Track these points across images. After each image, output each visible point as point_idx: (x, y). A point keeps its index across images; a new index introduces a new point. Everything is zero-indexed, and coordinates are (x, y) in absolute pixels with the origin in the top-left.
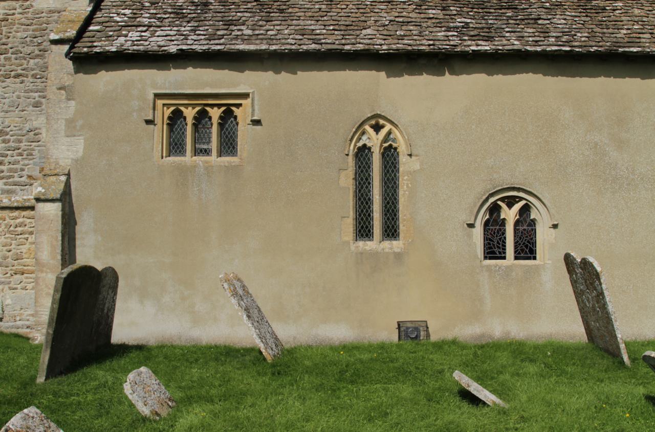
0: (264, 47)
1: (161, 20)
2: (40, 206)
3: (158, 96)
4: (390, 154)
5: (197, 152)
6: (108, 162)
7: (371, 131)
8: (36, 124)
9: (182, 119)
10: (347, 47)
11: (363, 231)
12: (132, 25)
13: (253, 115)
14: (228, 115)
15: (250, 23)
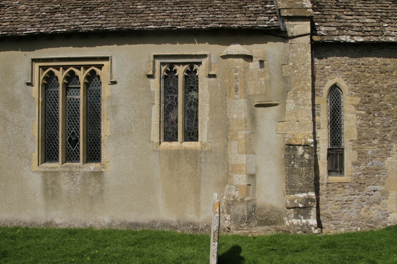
3: (156, 57)
6: (375, 142)
9: (76, 78)
13: (111, 78)
14: (92, 77)
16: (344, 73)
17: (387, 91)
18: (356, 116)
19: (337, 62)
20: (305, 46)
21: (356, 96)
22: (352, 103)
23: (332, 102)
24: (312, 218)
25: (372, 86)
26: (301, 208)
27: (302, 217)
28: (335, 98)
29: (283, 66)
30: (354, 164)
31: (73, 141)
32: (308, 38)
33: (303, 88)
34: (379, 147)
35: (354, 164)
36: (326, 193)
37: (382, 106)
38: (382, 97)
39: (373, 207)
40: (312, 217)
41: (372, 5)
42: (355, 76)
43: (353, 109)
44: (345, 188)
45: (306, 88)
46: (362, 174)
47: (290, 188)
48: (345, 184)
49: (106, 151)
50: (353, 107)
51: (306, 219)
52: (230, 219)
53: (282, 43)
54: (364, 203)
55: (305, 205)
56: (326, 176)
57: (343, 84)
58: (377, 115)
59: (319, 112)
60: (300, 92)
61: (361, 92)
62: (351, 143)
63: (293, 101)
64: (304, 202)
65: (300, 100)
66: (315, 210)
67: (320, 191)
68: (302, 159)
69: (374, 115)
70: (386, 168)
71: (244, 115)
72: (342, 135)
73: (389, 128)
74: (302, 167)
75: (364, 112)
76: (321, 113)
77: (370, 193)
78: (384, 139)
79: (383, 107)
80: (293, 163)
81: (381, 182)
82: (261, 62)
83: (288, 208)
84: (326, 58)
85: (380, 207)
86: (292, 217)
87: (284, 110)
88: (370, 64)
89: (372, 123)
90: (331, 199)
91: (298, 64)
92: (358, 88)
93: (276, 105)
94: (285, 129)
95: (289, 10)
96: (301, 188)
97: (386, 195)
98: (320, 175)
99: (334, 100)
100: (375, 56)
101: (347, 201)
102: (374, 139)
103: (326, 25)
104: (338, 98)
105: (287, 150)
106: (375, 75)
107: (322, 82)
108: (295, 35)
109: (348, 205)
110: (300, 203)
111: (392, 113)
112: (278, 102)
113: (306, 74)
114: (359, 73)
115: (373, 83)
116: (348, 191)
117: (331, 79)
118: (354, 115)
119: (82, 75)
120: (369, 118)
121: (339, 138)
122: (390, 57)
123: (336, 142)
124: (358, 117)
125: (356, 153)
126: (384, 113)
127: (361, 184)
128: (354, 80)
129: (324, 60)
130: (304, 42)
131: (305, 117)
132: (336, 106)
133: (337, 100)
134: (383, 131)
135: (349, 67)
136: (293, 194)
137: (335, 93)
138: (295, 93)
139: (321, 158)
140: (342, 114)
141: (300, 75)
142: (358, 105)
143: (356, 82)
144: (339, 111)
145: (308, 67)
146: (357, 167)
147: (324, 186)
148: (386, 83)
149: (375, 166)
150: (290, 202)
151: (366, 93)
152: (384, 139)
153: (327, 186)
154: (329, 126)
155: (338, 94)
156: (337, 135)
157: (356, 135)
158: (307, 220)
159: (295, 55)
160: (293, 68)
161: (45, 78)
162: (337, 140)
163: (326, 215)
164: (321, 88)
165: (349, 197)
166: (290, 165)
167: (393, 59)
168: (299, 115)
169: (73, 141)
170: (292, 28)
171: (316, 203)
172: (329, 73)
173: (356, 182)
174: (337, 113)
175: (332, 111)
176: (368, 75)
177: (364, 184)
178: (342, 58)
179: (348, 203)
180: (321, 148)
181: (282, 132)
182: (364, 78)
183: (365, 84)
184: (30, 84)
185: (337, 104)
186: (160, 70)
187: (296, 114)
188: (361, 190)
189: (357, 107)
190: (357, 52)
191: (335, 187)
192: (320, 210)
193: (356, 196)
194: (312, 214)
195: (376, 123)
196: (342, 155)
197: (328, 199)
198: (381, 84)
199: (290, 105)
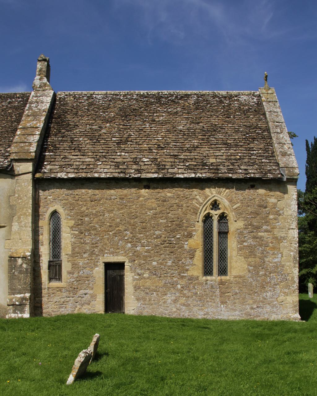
6: (85, 255)
16: (62, 202)
17: (96, 215)
18: (71, 235)
19: (57, 193)
20: (27, 181)
21: (71, 219)
22: (67, 225)
23: (54, 225)
24: (26, 313)
25: (83, 212)
26: (17, 305)
27: (19, 312)
28: (56, 221)
29: (11, 197)
30: (69, 273)
32: (30, 176)
33: (25, 214)
34: (88, 260)
35: (69, 273)
36: (47, 295)
37: (91, 227)
38: (92, 221)
39: (84, 307)
40: (26, 312)
41: (99, 146)
42: (71, 204)
43: (68, 230)
44: (62, 292)
45: (28, 214)
46: (75, 280)
47: (11, 290)
48: (62, 289)
50: (68, 228)
51: (21, 314)
53: (11, 179)
54: (77, 304)
55: (20, 303)
56: (47, 282)
57: (61, 210)
58: (87, 235)
59: (42, 232)
60: (23, 217)
61: (75, 217)
62: (67, 256)
63: (17, 224)
64: (20, 300)
65: (23, 223)
66: (29, 307)
67: (43, 294)
68: (21, 268)
69: (85, 235)
70: (94, 276)
72: (61, 250)
73: (97, 245)
74: (21, 274)
75: (77, 232)
76: (44, 233)
77: (82, 296)
78: (92, 253)
79: (92, 228)
80: (13, 271)
81: (90, 287)
83: (9, 305)
84: (49, 191)
85: (90, 307)
86: (11, 312)
87: (10, 231)
88: (83, 194)
89: (83, 241)
90: (51, 300)
91: (22, 195)
92: (73, 213)
93: (4, 227)
94: (11, 245)
95: (17, 154)
96: (20, 290)
97: (94, 298)
98: (42, 282)
99: (55, 223)
100: (86, 188)
101: (63, 302)
102: (85, 253)
103: (53, 164)
104: (58, 221)
105: (10, 261)
106: (87, 203)
107: (45, 209)
108: (20, 173)
109: (64, 305)
110: (17, 301)
111: (99, 233)
112: (6, 225)
113: (28, 203)
114: (74, 201)
115: (85, 209)
116: (65, 294)
117: (52, 207)
118: (69, 235)
120: (81, 237)
121: (58, 252)
122: (98, 189)
123: (56, 256)
124: (72, 236)
125: (70, 264)
126: (93, 233)
127: (75, 288)
128: (70, 207)
129: (47, 192)
130: (27, 178)
131: (27, 236)
132: (56, 228)
133: (57, 223)
134: (91, 247)
135: (66, 197)
136: (14, 295)
137: (56, 218)
138: (19, 218)
139: (43, 268)
140: (61, 234)
141: (23, 204)
142: (72, 227)
143: (71, 208)
144: (58, 231)
145: (29, 198)
146: (71, 275)
147: (46, 290)
148: (95, 209)
149: (85, 275)
150: (10, 301)
151: (79, 217)
152: (92, 253)
153: (48, 290)
154: (51, 243)
155: (58, 218)
156: (57, 250)
157: (70, 250)
158: (22, 315)
159: (20, 189)
160: (18, 198)
162: (57, 254)
163: (48, 313)
164: (44, 213)
165: (66, 299)
166: (12, 273)
167: (100, 190)
168: (22, 234)
170: (18, 168)
171: (29, 301)
172: (51, 201)
173: (71, 287)
174: (57, 233)
175: (54, 231)
176: (81, 203)
177: (77, 289)
178: (60, 190)
179: (65, 303)
180: (44, 260)
181: (8, 248)
182: (77, 205)
183: (78, 210)
185: (57, 226)
187: (19, 234)
188: (75, 293)
189: (71, 228)
190: (72, 185)
191: (54, 291)
192: (43, 309)
193: (71, 298)
194: (26, 310)
195: (86, 241)
196: (60, 266)
197: (49, 300)
198: (91, 210)
199: (15, 227)
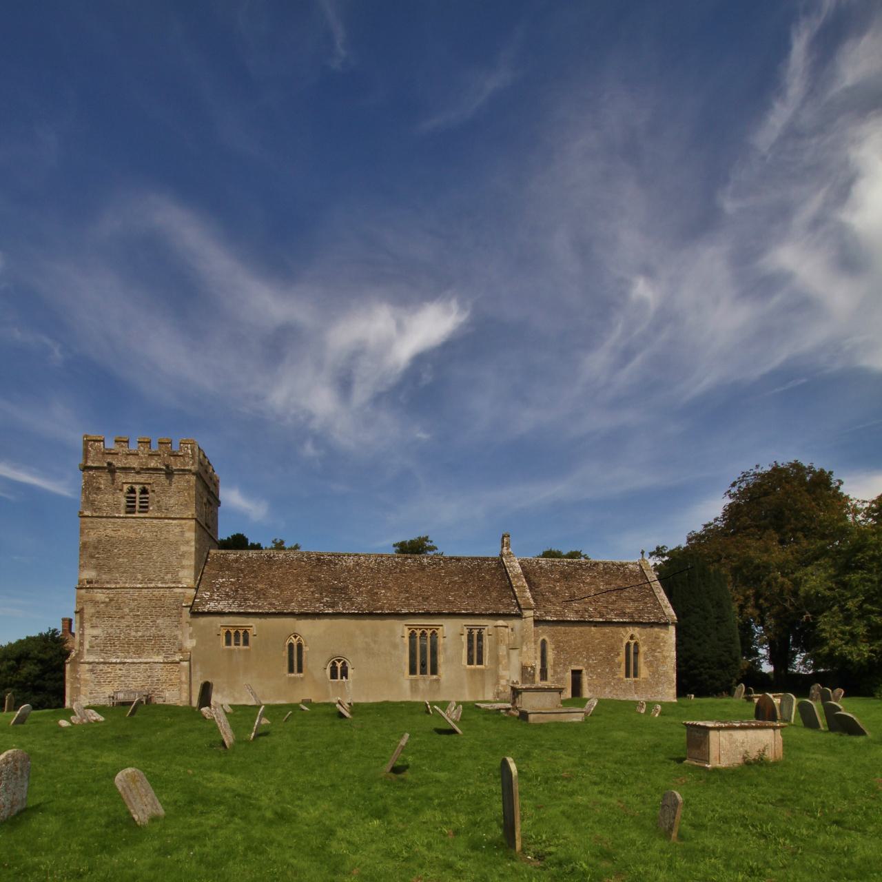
0: (257, 611)
1: (221, 597)
2: (182, 663)
4: (300, 646)
5: (236, 644)
6: (561, 666)
7: (293, 638)
8: (176, 633)
10: (285, 611)
11: (291, 670)
12: (211, 599)
14: (434, 634)
15: (253, 600)
30: (552, 676)
31: (423, 665)
49: (442, 670)
52: (157, 847)
57: (547, 639)
71: (505, 653)
82: (512, 629)
119: (429, 633)
138: (526, 644)
161: (410, 634)
169: (423, 665)
184: (403, 637)
186: (466, 632)
199: (525, 649)
